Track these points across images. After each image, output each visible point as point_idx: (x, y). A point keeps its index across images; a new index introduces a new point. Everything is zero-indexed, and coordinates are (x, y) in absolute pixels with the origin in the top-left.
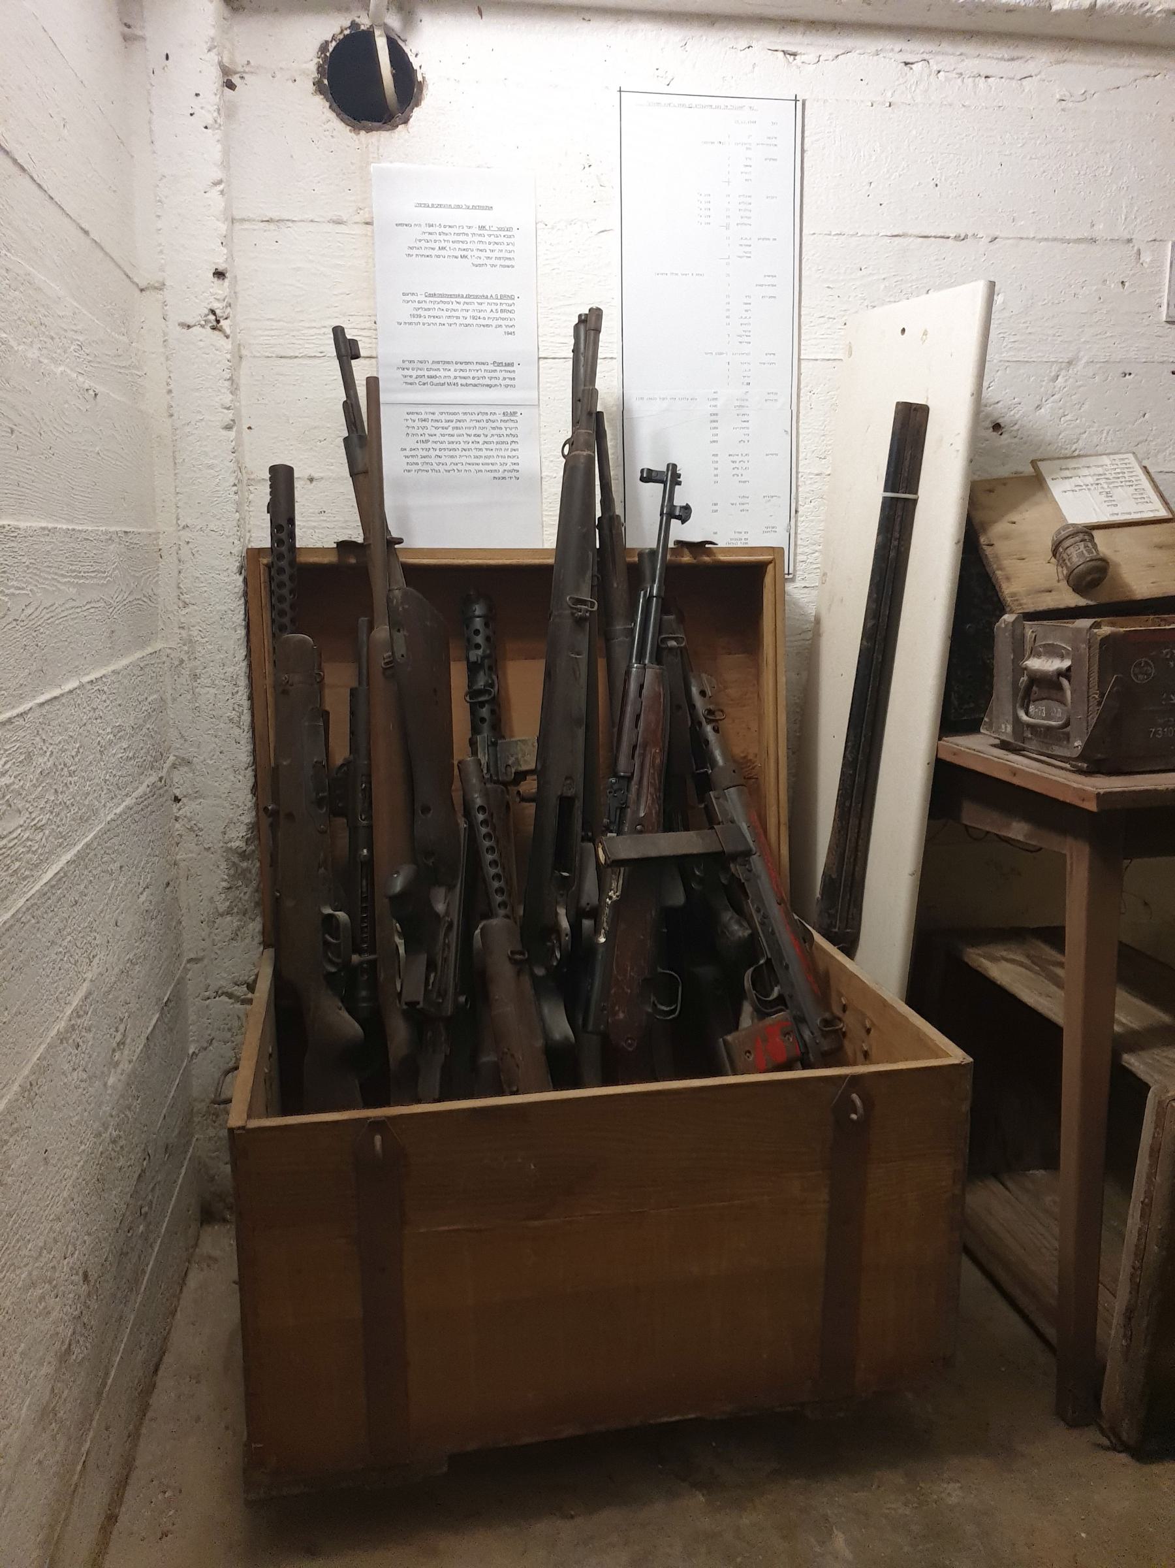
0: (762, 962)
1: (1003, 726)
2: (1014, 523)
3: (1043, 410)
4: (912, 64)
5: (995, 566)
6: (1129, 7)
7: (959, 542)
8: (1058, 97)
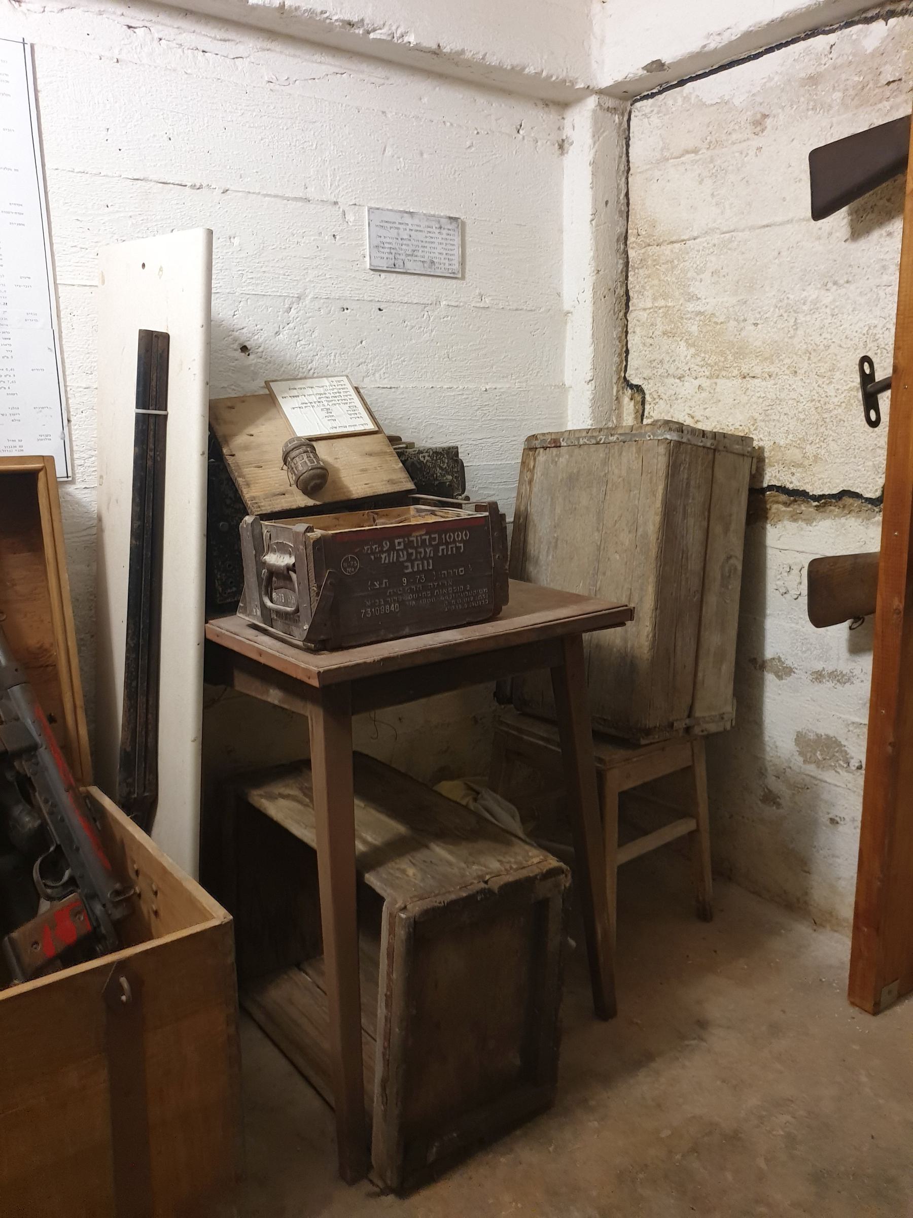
0: (52, 849)
1: (254, 610)
3: (281, 335)
4: (135, 28)
5: (236, 474)
6: (311, 11)
8: (266, 79)
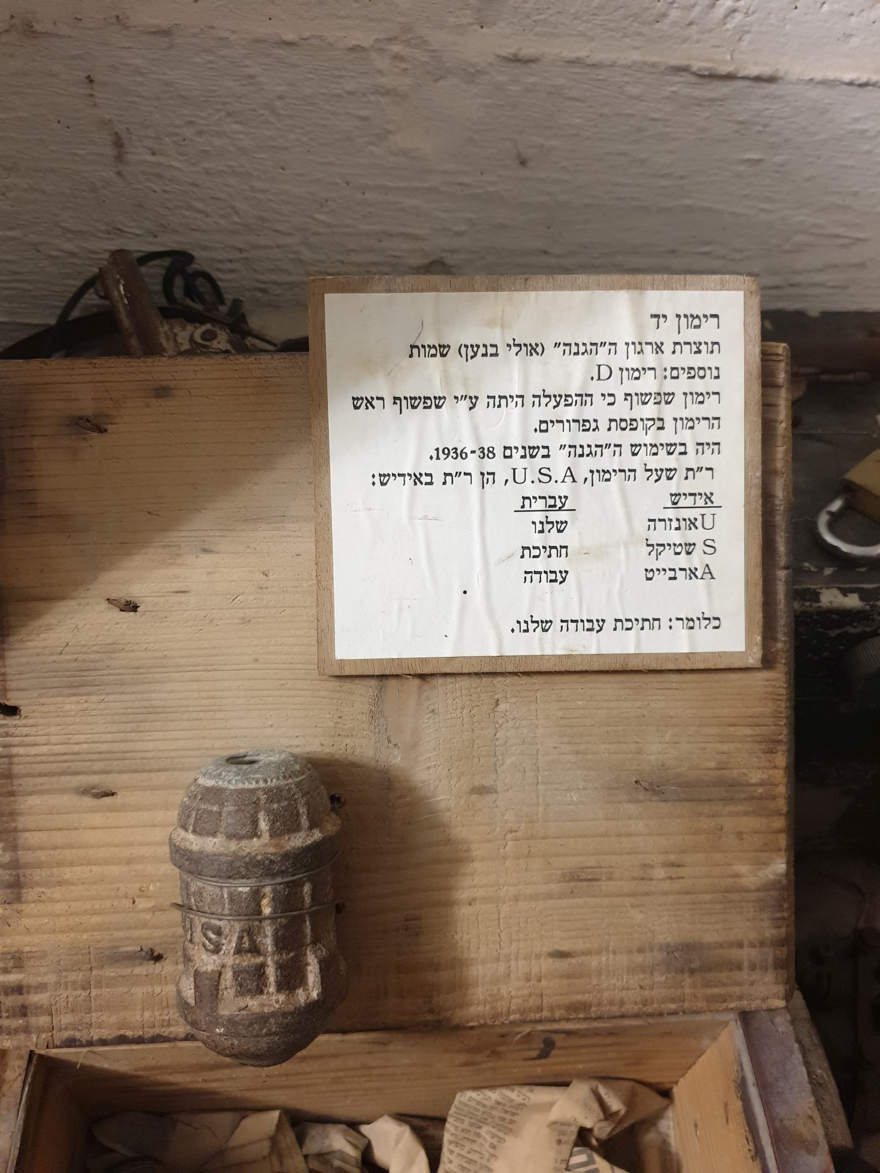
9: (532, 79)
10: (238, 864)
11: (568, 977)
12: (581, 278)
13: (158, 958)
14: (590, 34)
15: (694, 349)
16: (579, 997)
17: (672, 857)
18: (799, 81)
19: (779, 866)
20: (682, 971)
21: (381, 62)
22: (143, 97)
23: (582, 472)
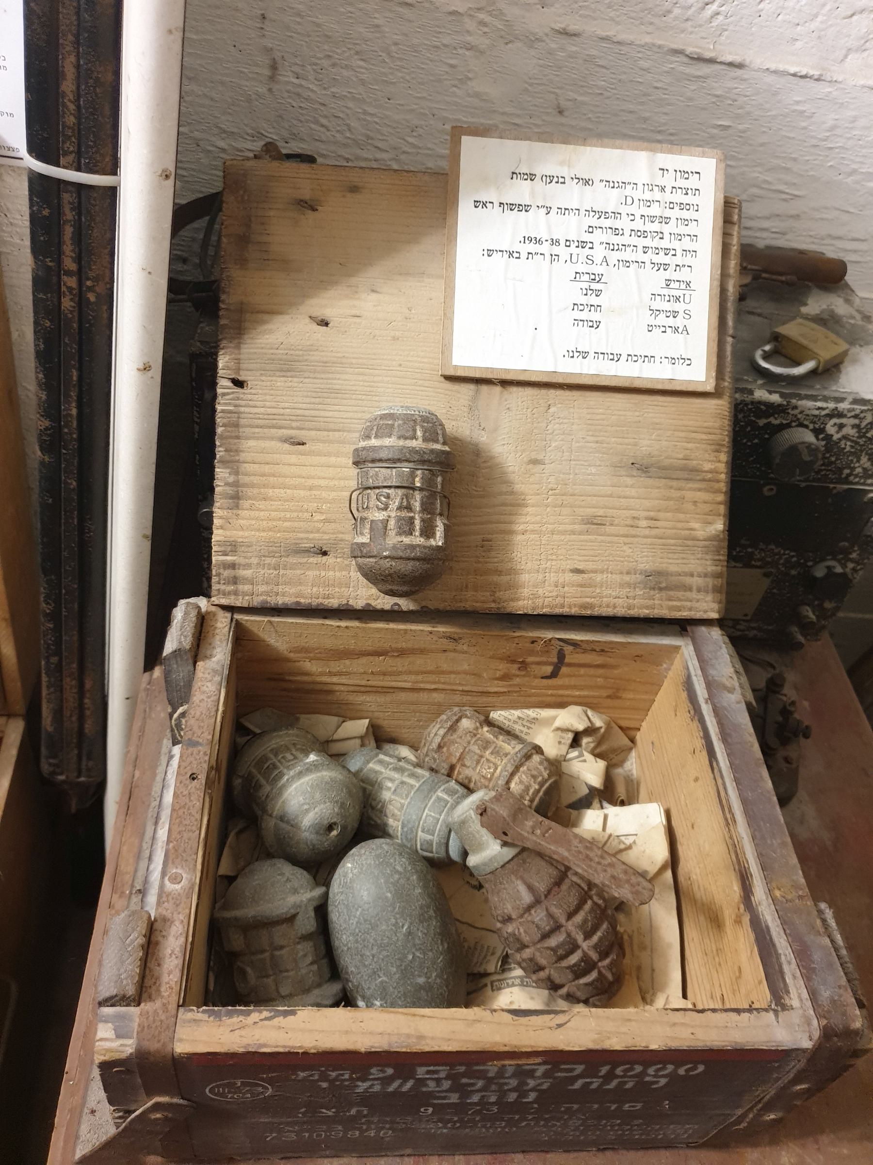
2: (327, 324)
7: (146, 368)
9: (574, 49)
10: (405, 451)
11: (581, 586)
12: (618, 142)
13: (325, 553)
14: (618, 19)
15: (684, 192)
16: (588, 600)
17: (652, 514)
18: (759, 70)
19: (719, 526)
20: (654, 589)
21: (470, 25)
22: (298, 33)
23: (613, 260)
